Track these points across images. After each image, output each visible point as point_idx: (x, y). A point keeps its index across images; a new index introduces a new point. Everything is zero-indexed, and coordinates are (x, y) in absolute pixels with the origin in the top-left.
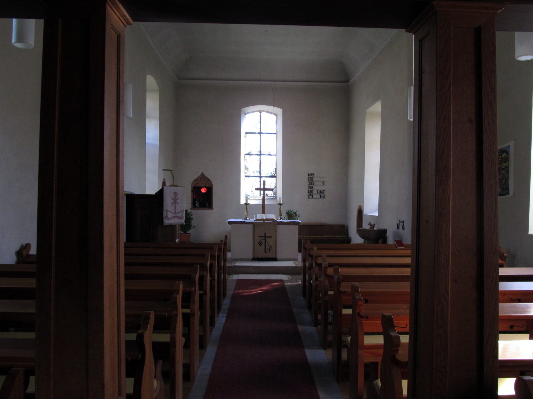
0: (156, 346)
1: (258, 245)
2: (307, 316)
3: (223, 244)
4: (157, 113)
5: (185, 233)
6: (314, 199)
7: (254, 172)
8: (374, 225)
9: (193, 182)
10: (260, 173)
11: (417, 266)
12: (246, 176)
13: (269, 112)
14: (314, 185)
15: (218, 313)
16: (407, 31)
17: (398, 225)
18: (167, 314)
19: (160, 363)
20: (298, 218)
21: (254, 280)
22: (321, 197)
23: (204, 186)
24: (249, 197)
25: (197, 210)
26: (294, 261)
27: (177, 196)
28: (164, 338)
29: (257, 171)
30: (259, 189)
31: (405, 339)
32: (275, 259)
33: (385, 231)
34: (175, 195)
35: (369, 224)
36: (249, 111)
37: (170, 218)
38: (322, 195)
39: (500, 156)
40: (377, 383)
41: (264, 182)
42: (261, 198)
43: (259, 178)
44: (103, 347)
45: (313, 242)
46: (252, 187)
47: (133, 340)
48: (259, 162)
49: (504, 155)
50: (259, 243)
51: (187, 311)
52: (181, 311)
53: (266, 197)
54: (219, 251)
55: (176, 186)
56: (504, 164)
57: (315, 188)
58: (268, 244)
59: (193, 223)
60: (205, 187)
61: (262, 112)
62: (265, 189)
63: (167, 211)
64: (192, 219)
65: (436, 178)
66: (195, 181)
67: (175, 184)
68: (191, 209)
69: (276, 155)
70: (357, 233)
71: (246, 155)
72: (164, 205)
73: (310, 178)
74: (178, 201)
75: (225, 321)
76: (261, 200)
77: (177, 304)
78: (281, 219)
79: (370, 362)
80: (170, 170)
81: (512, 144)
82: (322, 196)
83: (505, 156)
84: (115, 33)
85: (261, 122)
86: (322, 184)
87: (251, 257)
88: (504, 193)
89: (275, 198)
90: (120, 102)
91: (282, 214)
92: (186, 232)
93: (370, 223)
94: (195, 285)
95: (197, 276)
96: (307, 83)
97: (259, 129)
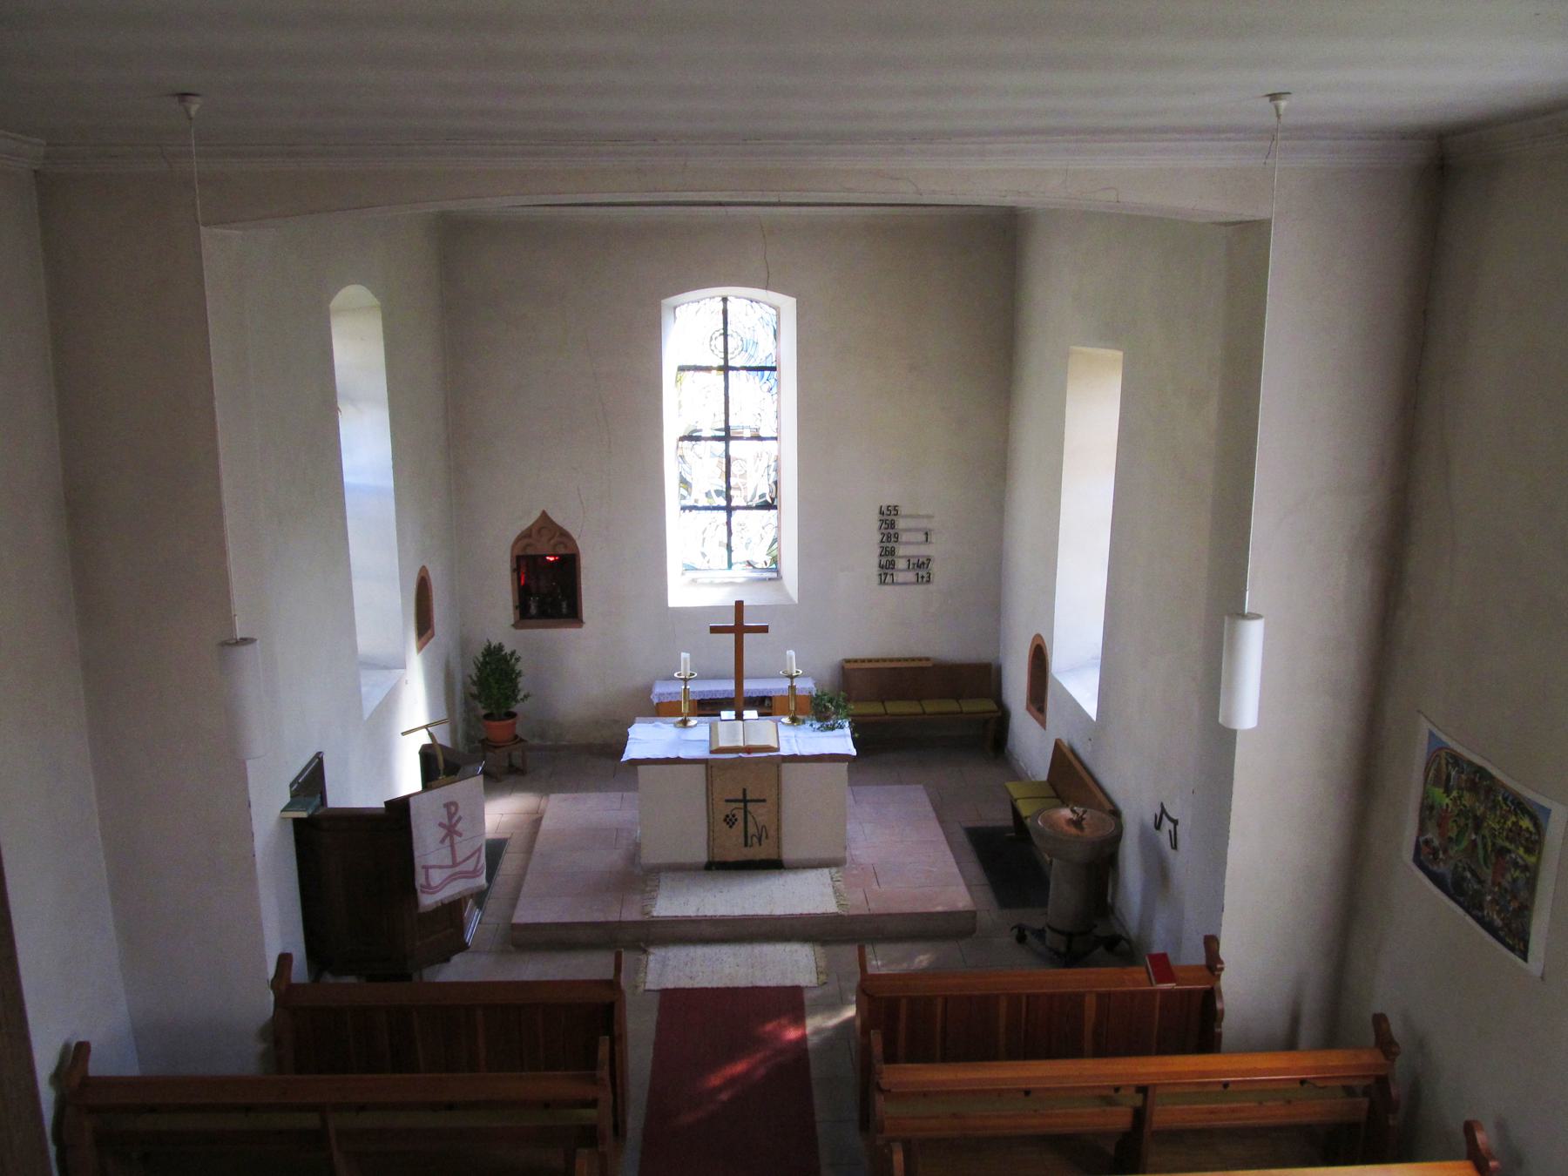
1: (725, 824)
10: (729, 498)
12: (684, 508)
14: (896, 542)
21: (712, 989)
22: (920, 580)
27: (455, 814)
32: (774, 865)
34: (449, 813)
37: (437, 887)
46: (704, 539)
48: (724, 460)
50: (725, 820)
57: (901, 551)
58: (756, 823)
63: (426, 868)
64: (519, 674)
70: (1028, 709)
71: (683, 439)
72: (416, 854)
74: (459, 827)
82: (923, 577)
86: (924, 538)
87: (703, 857)
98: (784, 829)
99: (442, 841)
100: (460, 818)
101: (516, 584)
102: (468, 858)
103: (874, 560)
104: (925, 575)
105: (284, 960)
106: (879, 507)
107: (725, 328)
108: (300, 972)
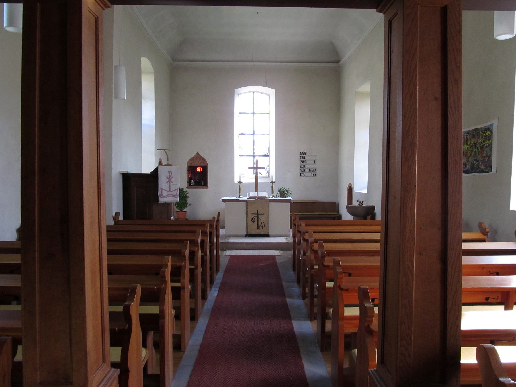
0: (143, 318)
1: (251, 222)
2: (296, 290)
3: (215, 221)
5: (181, 210)
6: (307, 177)
8: (363, 202)
9: (189, 161)
11: (386, 241)
13: (262, 93)
15: (211, 287)
16: (378, 11)
18: (156, 287)
19: (151, 334)
22: (312, 175)
23: (199, 165)
26: (285, 237)
28: (154, 310)
30: (253, 168)
31: (376, 310)
32: (267, 236)
33: (373, 208)
35: (358, 201)
37: (164, 196)
38: (313, 173)
39: (484, 134)
40: (354, 352)
41: (257, 162)
44: (85, 317)
45: (301, 219)
47: (120, 311)
49: (488, 133)
50: (251, 220)
51: (178, 285)
52: (169, 285)
53: (259, 175)
54: (210, 227)
55: (171, 165)
56: (488, 142)
57: (307, 166)
59: (189, 201)
60: (200, 166)
61: (255, 92)
62: (257, 168)
63: (162, 189)
64: (188, 197)
65: (402, 155)
66: (190, 160)
67: (170, 164)
75: (217, 294)
77: (166, 278)
78: (273, 196)
79: (351, 333)
80: (164, 150)
81: (495, 122)
83: (489, 134)
84: (92, 16)
85: (254, 103)
87: (245, 234)
88: (487, 170)
89: (269, 177)
90: (99, 83)
91: (274, 191)
94: (185, 260)
95: (187, 253)
98: (270, 223)
99: (167, 183)
100: (172, 177)
101: (188, 176)
102: (174, 191)
104: (315, 174)
105: (117, 214)
108: (121, 218)
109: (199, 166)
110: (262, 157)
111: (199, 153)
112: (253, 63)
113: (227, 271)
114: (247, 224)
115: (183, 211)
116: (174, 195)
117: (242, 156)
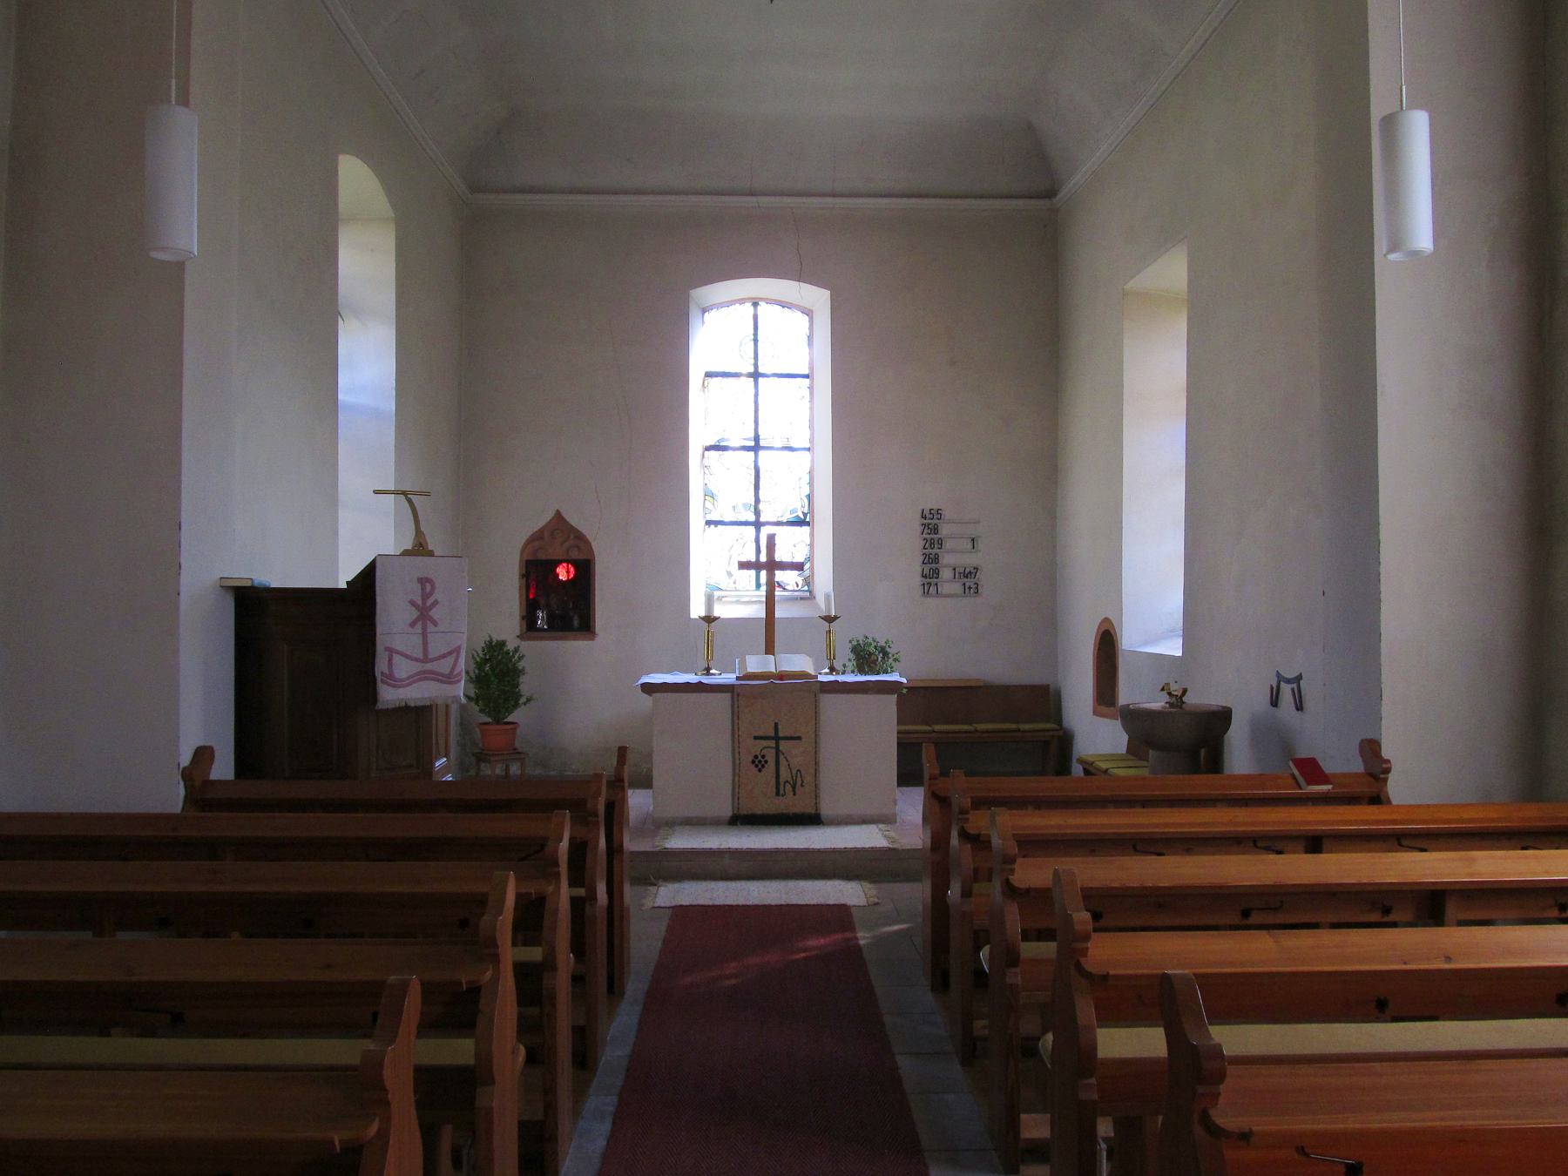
4: (387, 298)
7: (734, 508)
10: (757, 513)
12: (709, 523)
13: (783, 304)
17: (1274, 690)
20: (892, 668)
22: (966, 590)
23: (565, 557)
24: (717, 594)
25: (542, 639)
26: (881, 826)
27: (431, 594)
28: (457, 1051)
29: (744, 505)
30: (754, 566)
32: (812, 819)
33: (1222, 717)
34: (423, 589)
35: (1163, 689)
36: (717, 301)
37: (401, 680)
38: (970, 582)
42: (761, 596)
43: (752, 529)
48: (753, 472)
50: (753, 762)
51: (535, 954)
52: (510, 954)
53: (778, 593)
57: (947, 559)
59: (526, 686)
60: (568, 562)
62: (772, 566)
64: (522, 672)
68: (518, 637)
69: (809, 449)
71: (708, 448)
72: (379, 630)
73: (929, 524)
74: (434, 613)
76: (760, 602)
78: (832, 670)
80: (404, 493)
82: (970, 588)
86: (970, 545)
87: (727, 812)
89: (811, 596)
91: (834, 651)
92: (504, 719)
93: (1168, 684)
96: (913, 201)
97: (752, 361)
99: (413, 625)
100: (435, 603)
101: (524, 597)
102: (444, 656)
103: (917, 567)
104: (973, 586)
105: (204, 755)
106: (920, 512)
107: (756, 334)
108: (223, 769)
109: (565, 561)
110: (785, 527)
111: (565, 514)
112: (754, 199)
113: (656, 996)
114: (737, 778)
115: (505, 720)
116: (443, 675)
117: (717, 523)
